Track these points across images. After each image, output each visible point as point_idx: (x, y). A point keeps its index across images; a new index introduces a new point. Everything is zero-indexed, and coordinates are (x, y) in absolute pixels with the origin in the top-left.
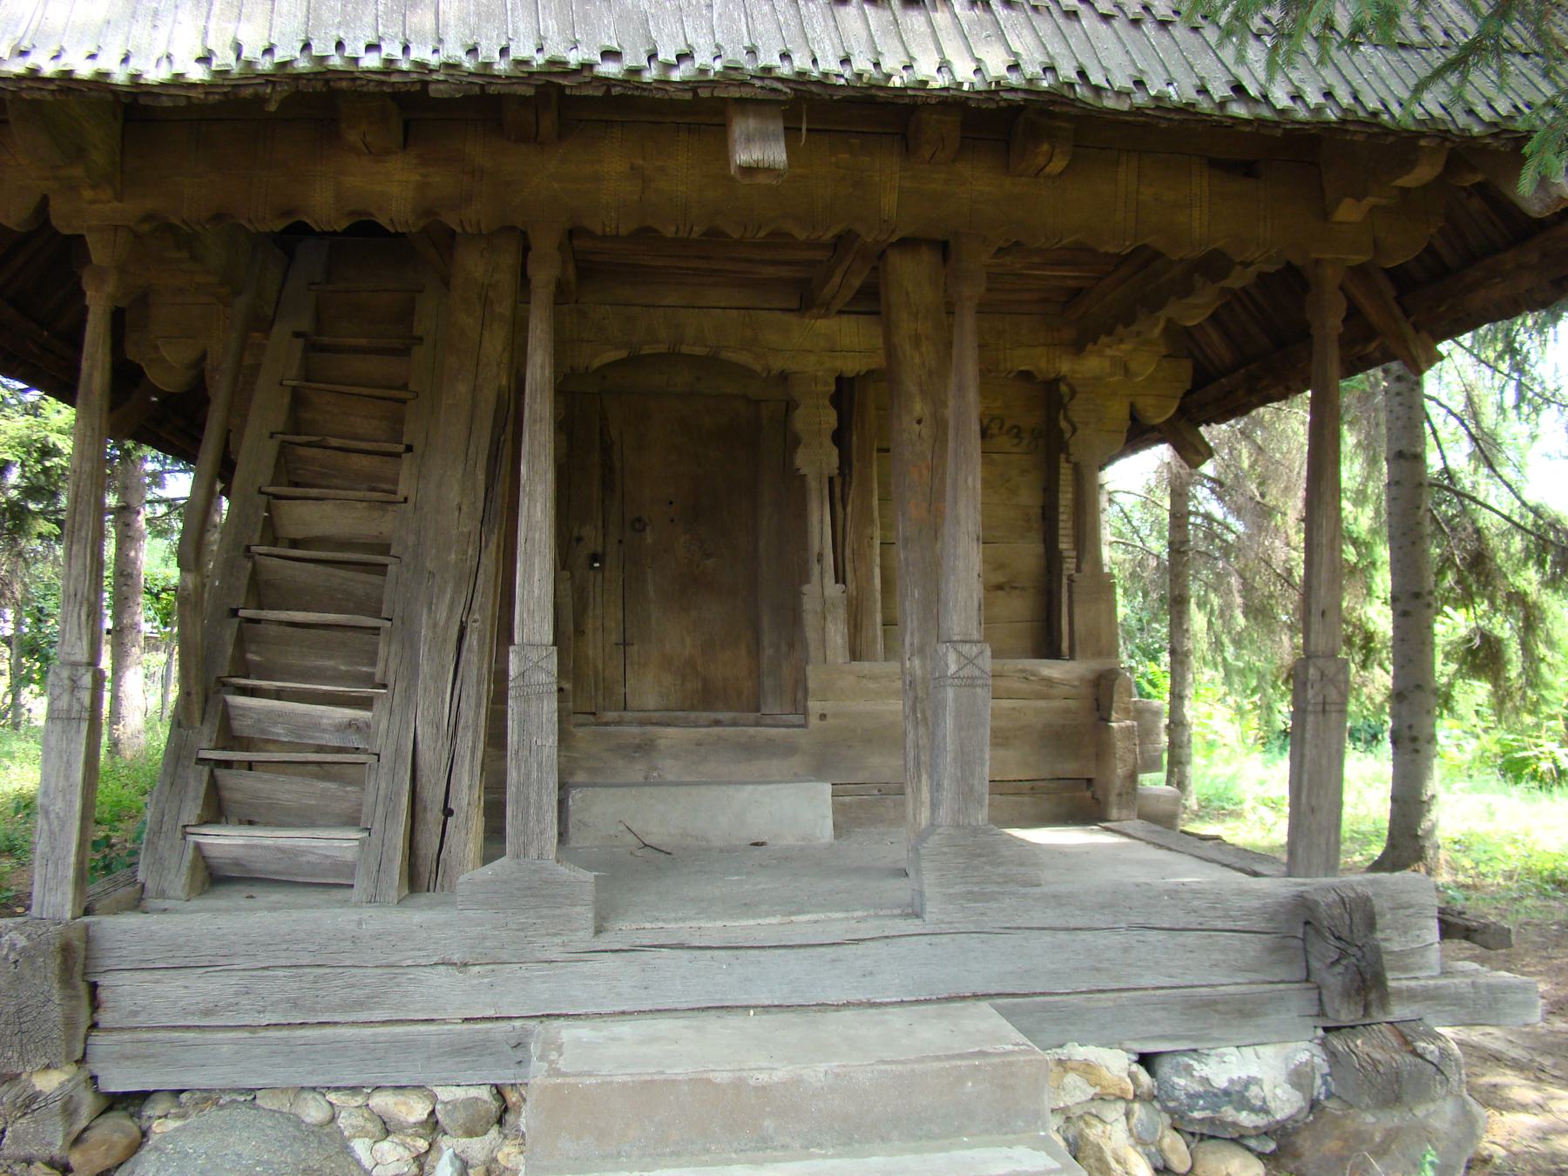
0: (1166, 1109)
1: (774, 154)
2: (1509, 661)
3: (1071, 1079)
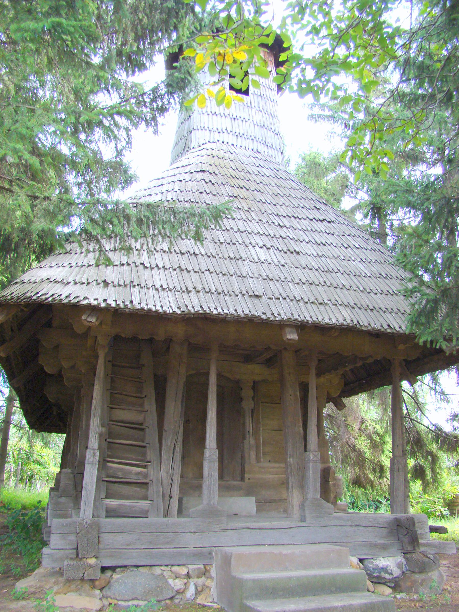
1: (294, 336)
2: (427, 474)
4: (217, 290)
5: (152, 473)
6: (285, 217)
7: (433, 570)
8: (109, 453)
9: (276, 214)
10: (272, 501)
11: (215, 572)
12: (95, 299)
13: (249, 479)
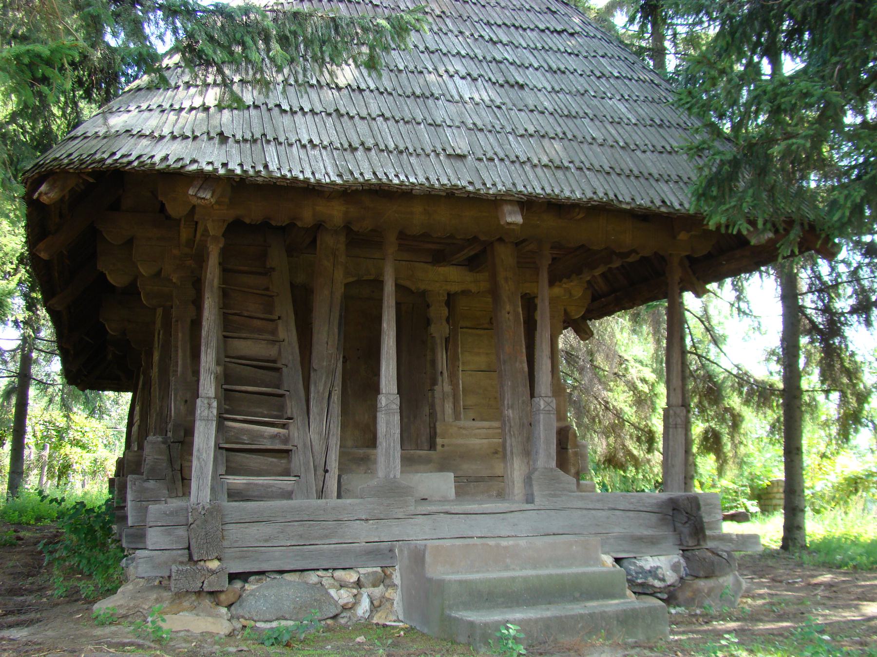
1: (518, 219)
4: (397, 147)
5: (296, 435)
6: (499, 26)
7: (726, 574)
8: (227, 407)
9: (485, 21)
10: (479, 480)
11: (399, 577)
12: (209, 163)
13: (443, 446)
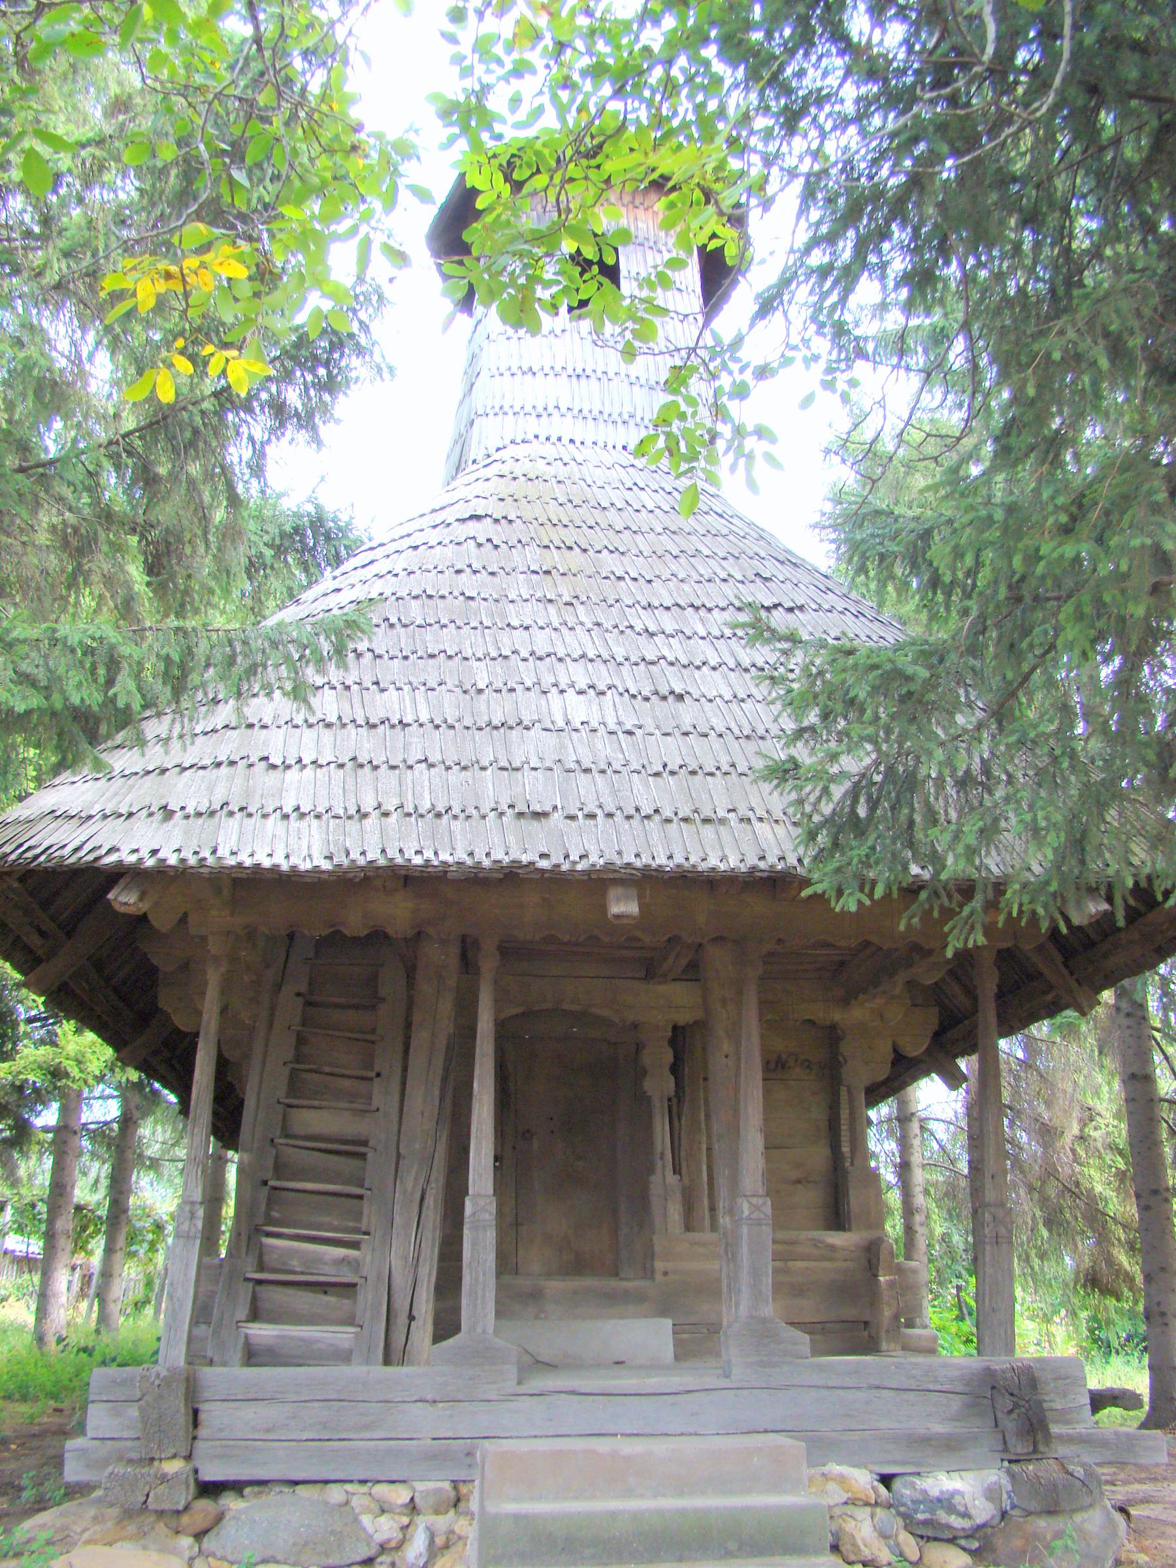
0: (899, 1514)
3: (831, 1486)
6: (668, 608)
